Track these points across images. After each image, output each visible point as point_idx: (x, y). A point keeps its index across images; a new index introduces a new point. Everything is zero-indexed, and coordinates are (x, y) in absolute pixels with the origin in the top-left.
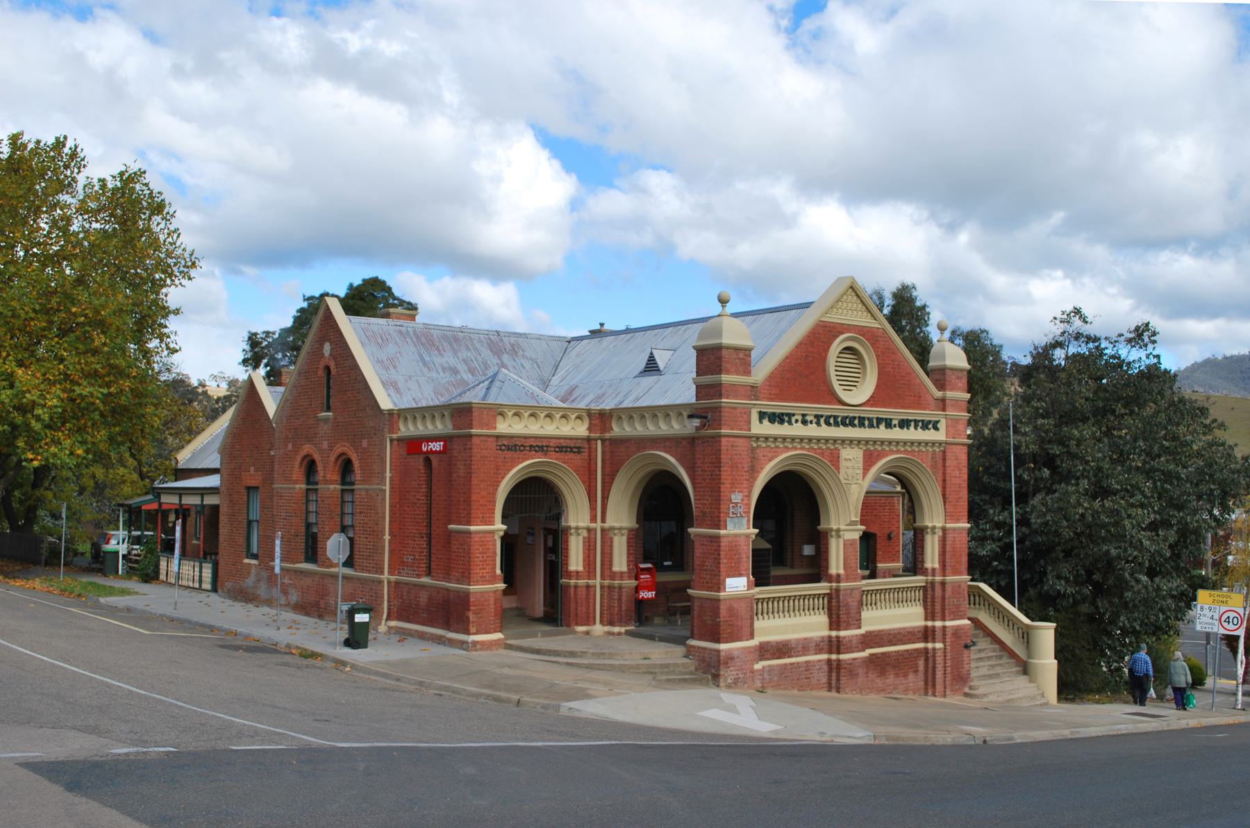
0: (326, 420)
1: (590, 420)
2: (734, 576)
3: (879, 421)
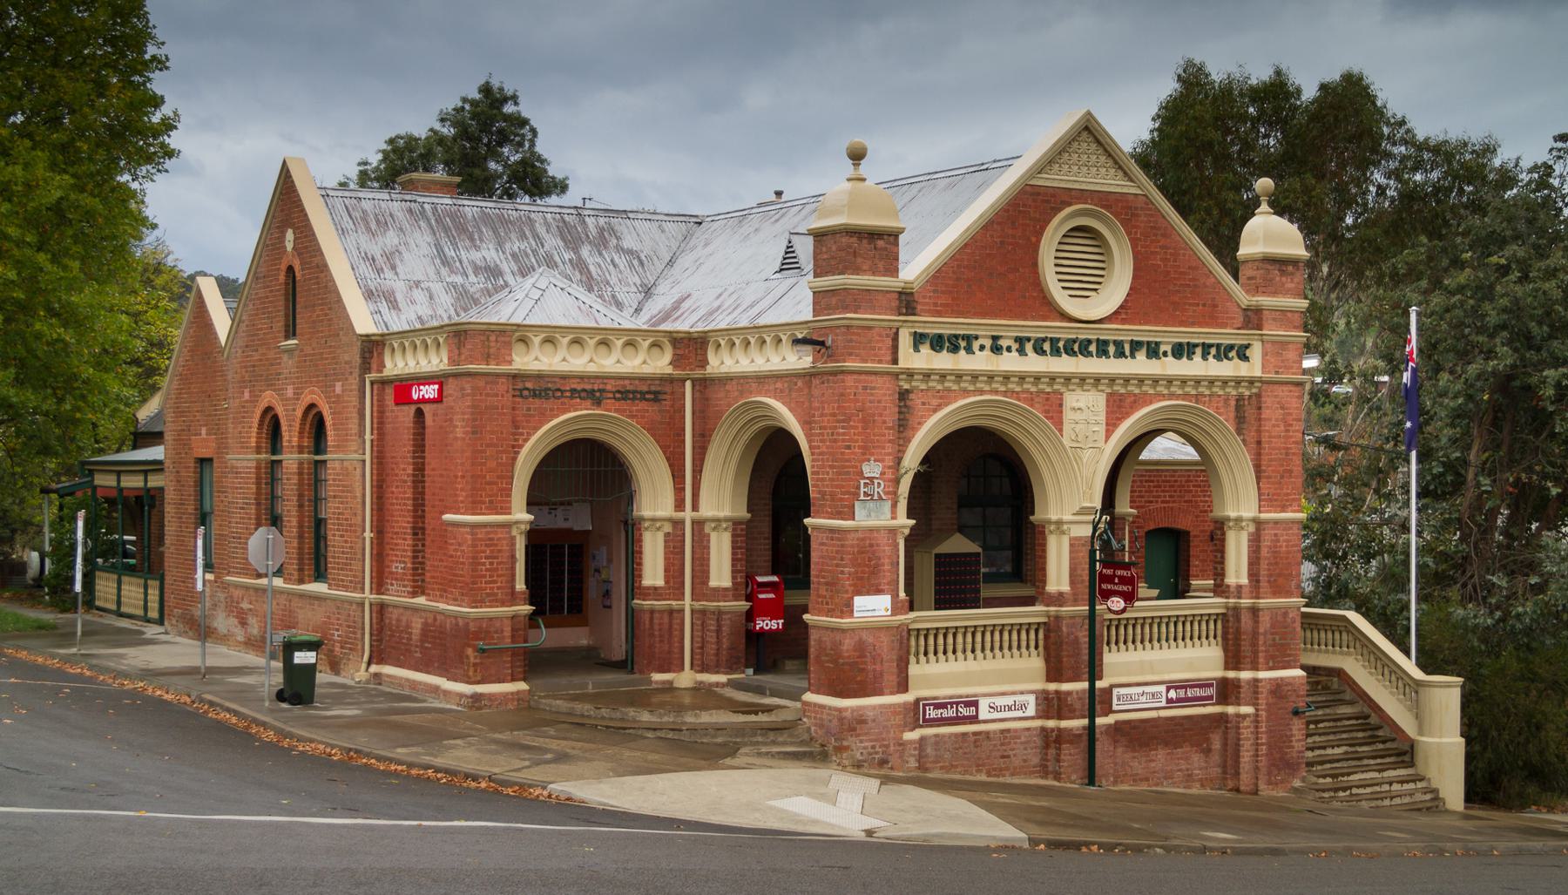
0: (290, 351)
1: (675, 347)
2: (868, 593)
3: (1136, 346)
